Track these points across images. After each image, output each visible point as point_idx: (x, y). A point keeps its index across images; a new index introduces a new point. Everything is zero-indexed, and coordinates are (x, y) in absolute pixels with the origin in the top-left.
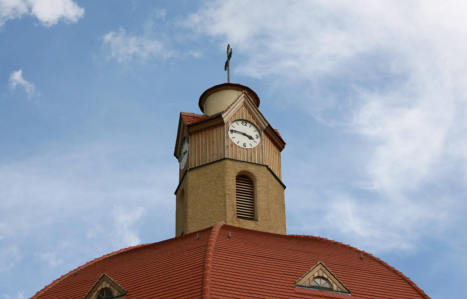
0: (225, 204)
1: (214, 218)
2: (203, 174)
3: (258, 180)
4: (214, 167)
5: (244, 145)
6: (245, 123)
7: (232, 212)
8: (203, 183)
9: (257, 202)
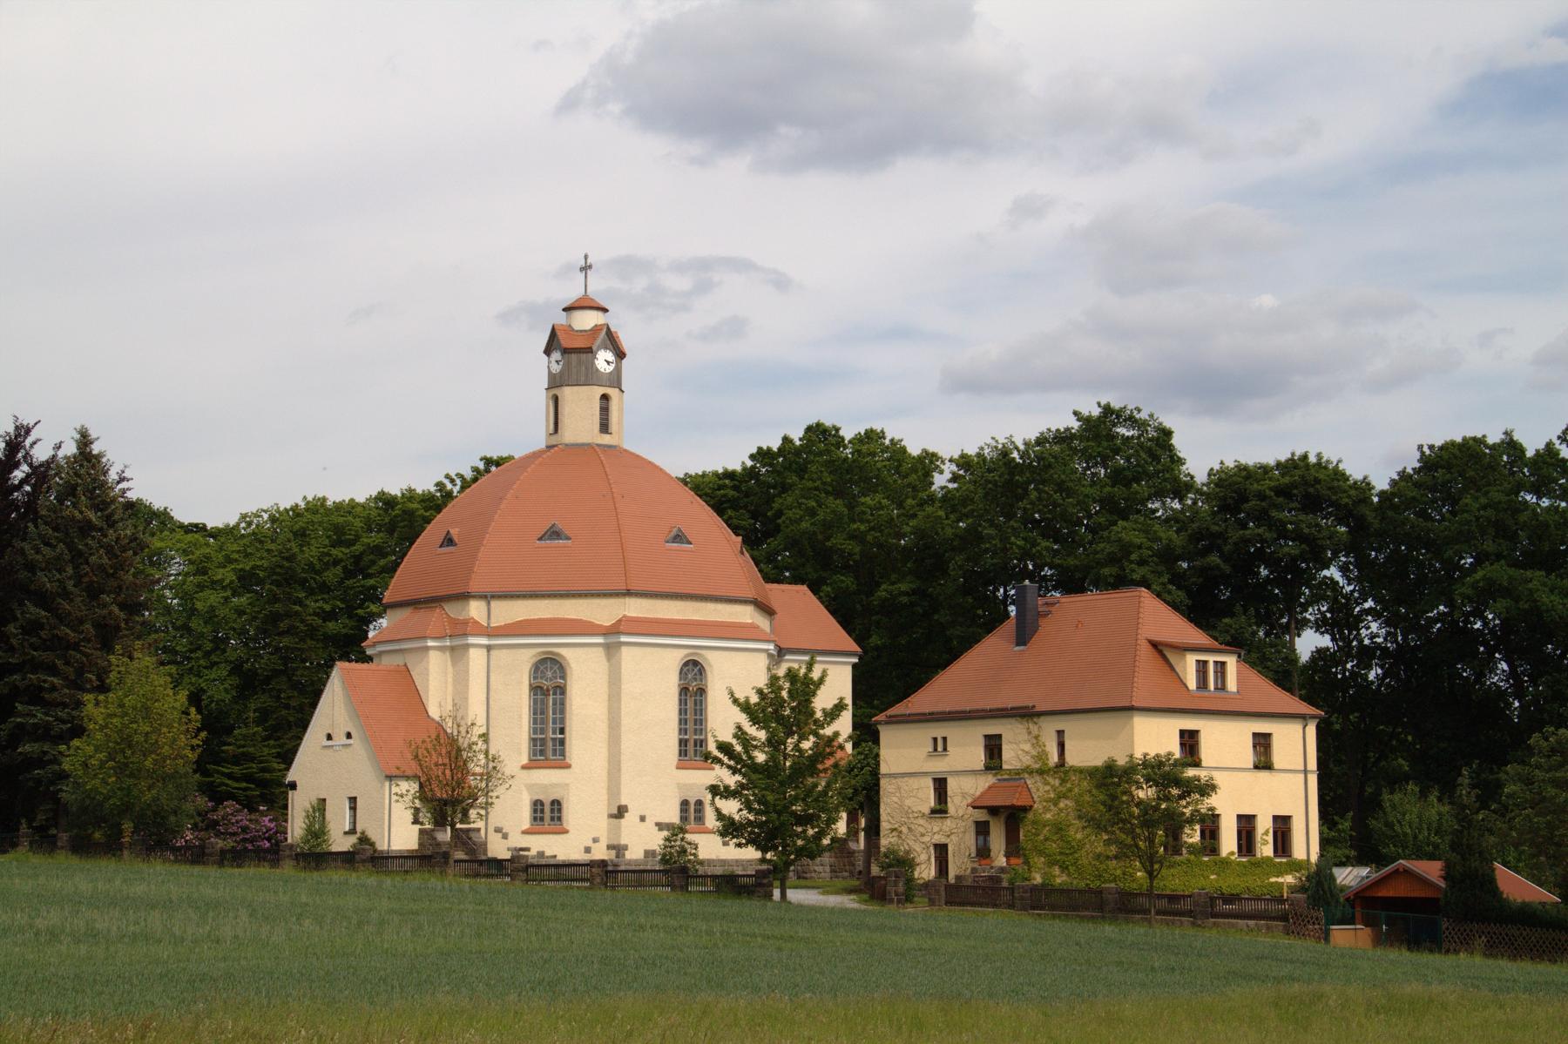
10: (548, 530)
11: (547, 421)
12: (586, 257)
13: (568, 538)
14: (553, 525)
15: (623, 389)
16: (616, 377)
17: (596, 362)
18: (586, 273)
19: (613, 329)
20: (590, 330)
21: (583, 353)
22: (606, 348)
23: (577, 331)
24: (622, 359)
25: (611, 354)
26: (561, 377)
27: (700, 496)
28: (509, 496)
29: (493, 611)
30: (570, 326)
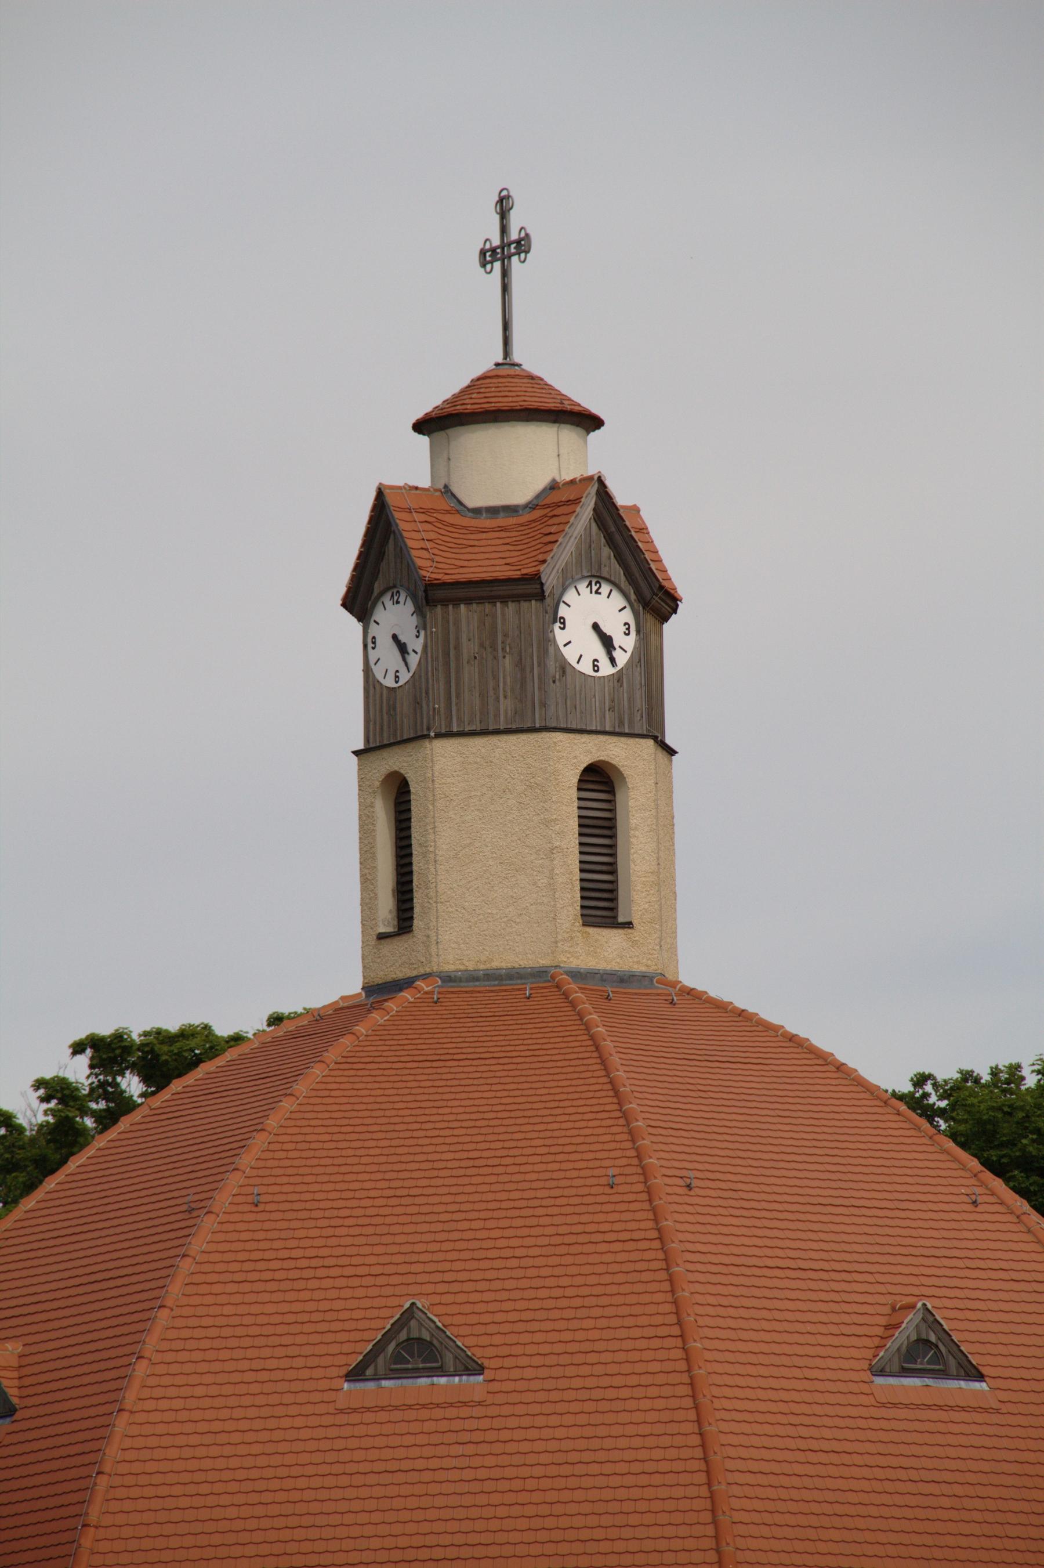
0: (552, 881)
1: (518, 920)
2: (478, 760)
3: (633, 788)
4: (513, 748)
5: (594, 666)
6: (597, 583)
7: (570, 909)
8: (479, 794)
9: (631, 863)
10: (388, 1337)
11: (367, 881)
12: (504, 206)
13: (472, 1367)
14: (410, 1313)
15: (669, 741)
16: (640, 702)
17: (560, 636)
18: (505, 274)
19: (622, 498)
20: (532, 506)
21: (505, 600)
22: (596, 578)
23: (477, 511)
24: (665, 619)
25: (618, 600)
26: (417, 703)
27: (999, 1170)
28: (223, 1200)
29: (560, 438)
30: (447, 491)
